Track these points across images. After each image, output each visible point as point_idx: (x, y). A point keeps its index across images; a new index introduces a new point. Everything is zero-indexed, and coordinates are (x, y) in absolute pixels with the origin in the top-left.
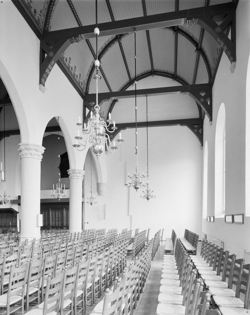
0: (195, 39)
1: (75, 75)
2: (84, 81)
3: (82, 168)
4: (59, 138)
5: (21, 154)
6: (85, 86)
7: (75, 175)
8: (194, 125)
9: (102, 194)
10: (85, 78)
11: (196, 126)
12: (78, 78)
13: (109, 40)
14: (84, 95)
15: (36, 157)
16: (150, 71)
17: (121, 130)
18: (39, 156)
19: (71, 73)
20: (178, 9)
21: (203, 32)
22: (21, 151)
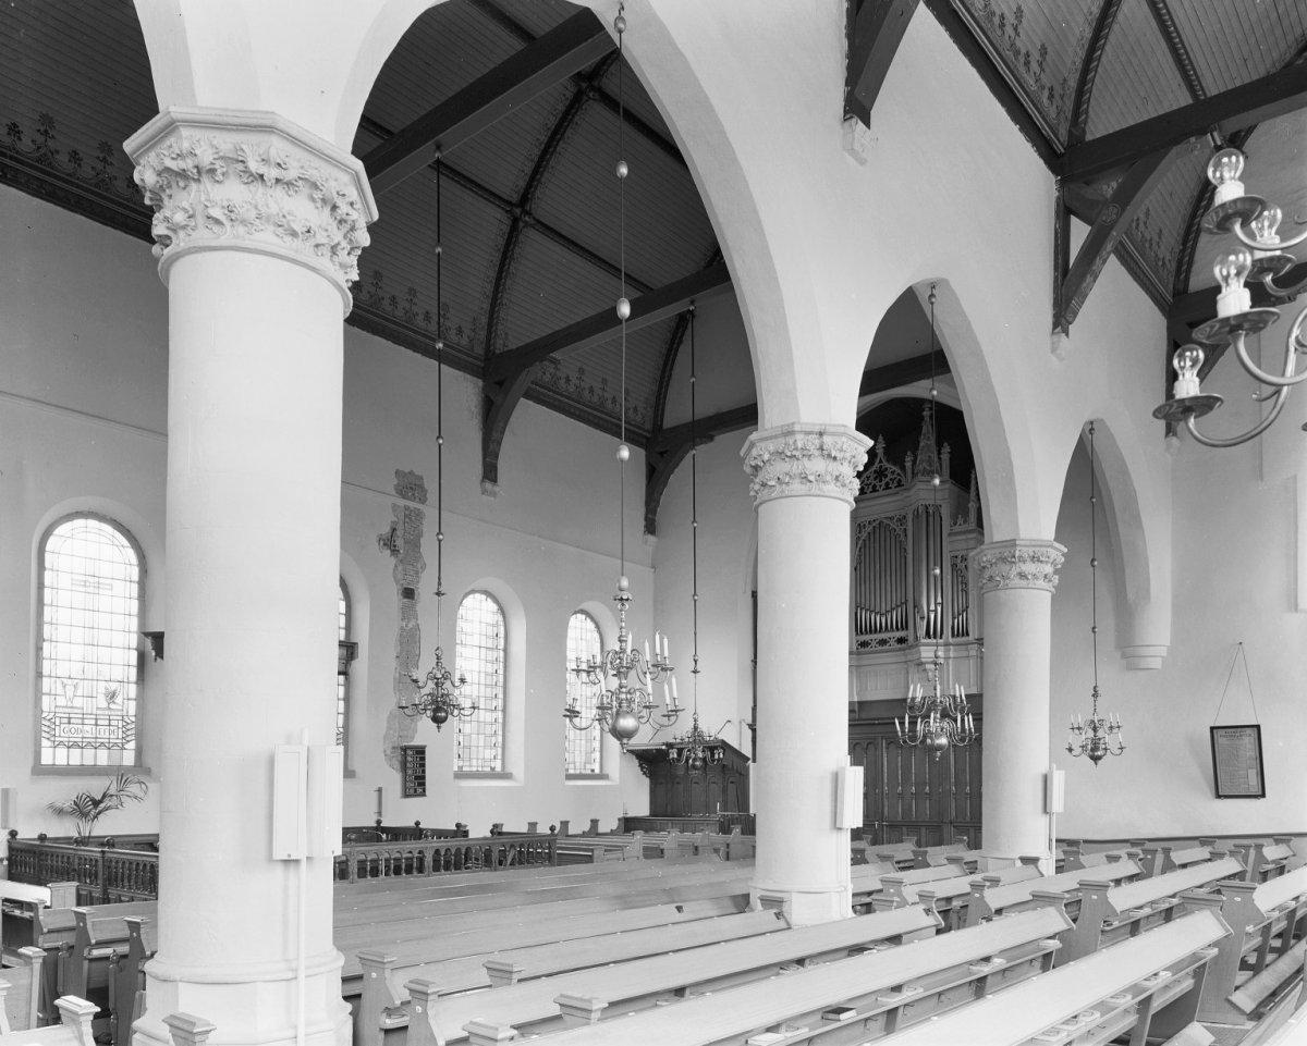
1: (993, 14)
2: (1065, 80)
3: (1047, 529)
4: (624, 170)
5: (757, 487)
6: (1069, 104)
7: (1014, 571)
9: (1151, 648)
12: (1034, 66)
15: (831, 488)
18: (844, 485)
19: (1004, 46)
22: (756, 468)
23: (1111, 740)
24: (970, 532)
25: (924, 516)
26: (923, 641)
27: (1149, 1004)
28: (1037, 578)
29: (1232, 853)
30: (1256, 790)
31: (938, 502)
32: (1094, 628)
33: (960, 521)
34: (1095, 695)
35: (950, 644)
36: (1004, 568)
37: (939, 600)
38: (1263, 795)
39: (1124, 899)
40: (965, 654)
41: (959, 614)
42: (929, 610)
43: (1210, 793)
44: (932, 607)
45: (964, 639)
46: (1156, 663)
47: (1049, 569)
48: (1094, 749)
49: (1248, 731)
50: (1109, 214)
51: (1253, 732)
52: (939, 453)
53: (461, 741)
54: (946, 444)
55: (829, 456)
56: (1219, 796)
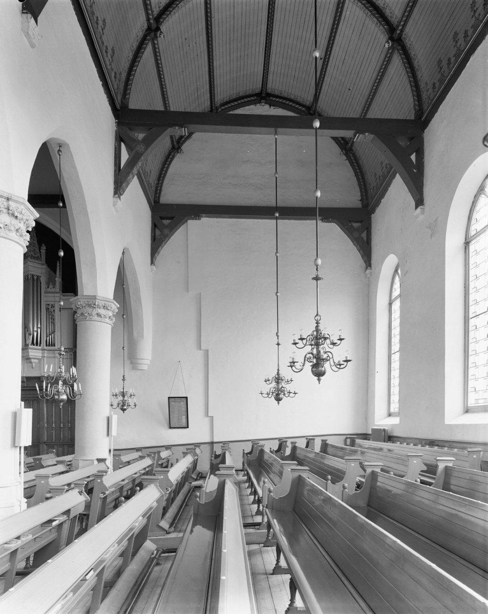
0: (388, 13)
3: (111, 295)
6: (122, 86)
7: (95, 312)
8: (350, 221)
9: (143, 360)
10: (127, 54)
11: (356, 225)
13: (143, 27)
14: (118, 107)
16: (258, 91)
17: (189, 221)
20: (366, 114)
21: (164, 166)
23: (131, 401)
24: (57, 293)
25: (32, 280)
26: (30, 346)
27: (62, 526)
28: (106, 317)
29: (148, 456)
30: (185, 425)
31: (39, 275)
32: (123, 347)
33: (51, 286)
34: (124, 380)
35: (45, 350)
36: (90, 310)
37: (39, 326)
38: (188, 427)
39: (55, 482)
40: (52, 355)
41: (50, 335)
42: (33, 331)
43: (167, 426)
44: (35, 329)
45: (53, 348)
46: (145, 367)
47: (110, 314)
48: (123, 405)
49: (183, 399)
50: (140, 148)
51: (184, 400)
52: (40, 249)
53: (188, 47)
54: (43, 245)
55: (13, 215)
56: (170, 428)
